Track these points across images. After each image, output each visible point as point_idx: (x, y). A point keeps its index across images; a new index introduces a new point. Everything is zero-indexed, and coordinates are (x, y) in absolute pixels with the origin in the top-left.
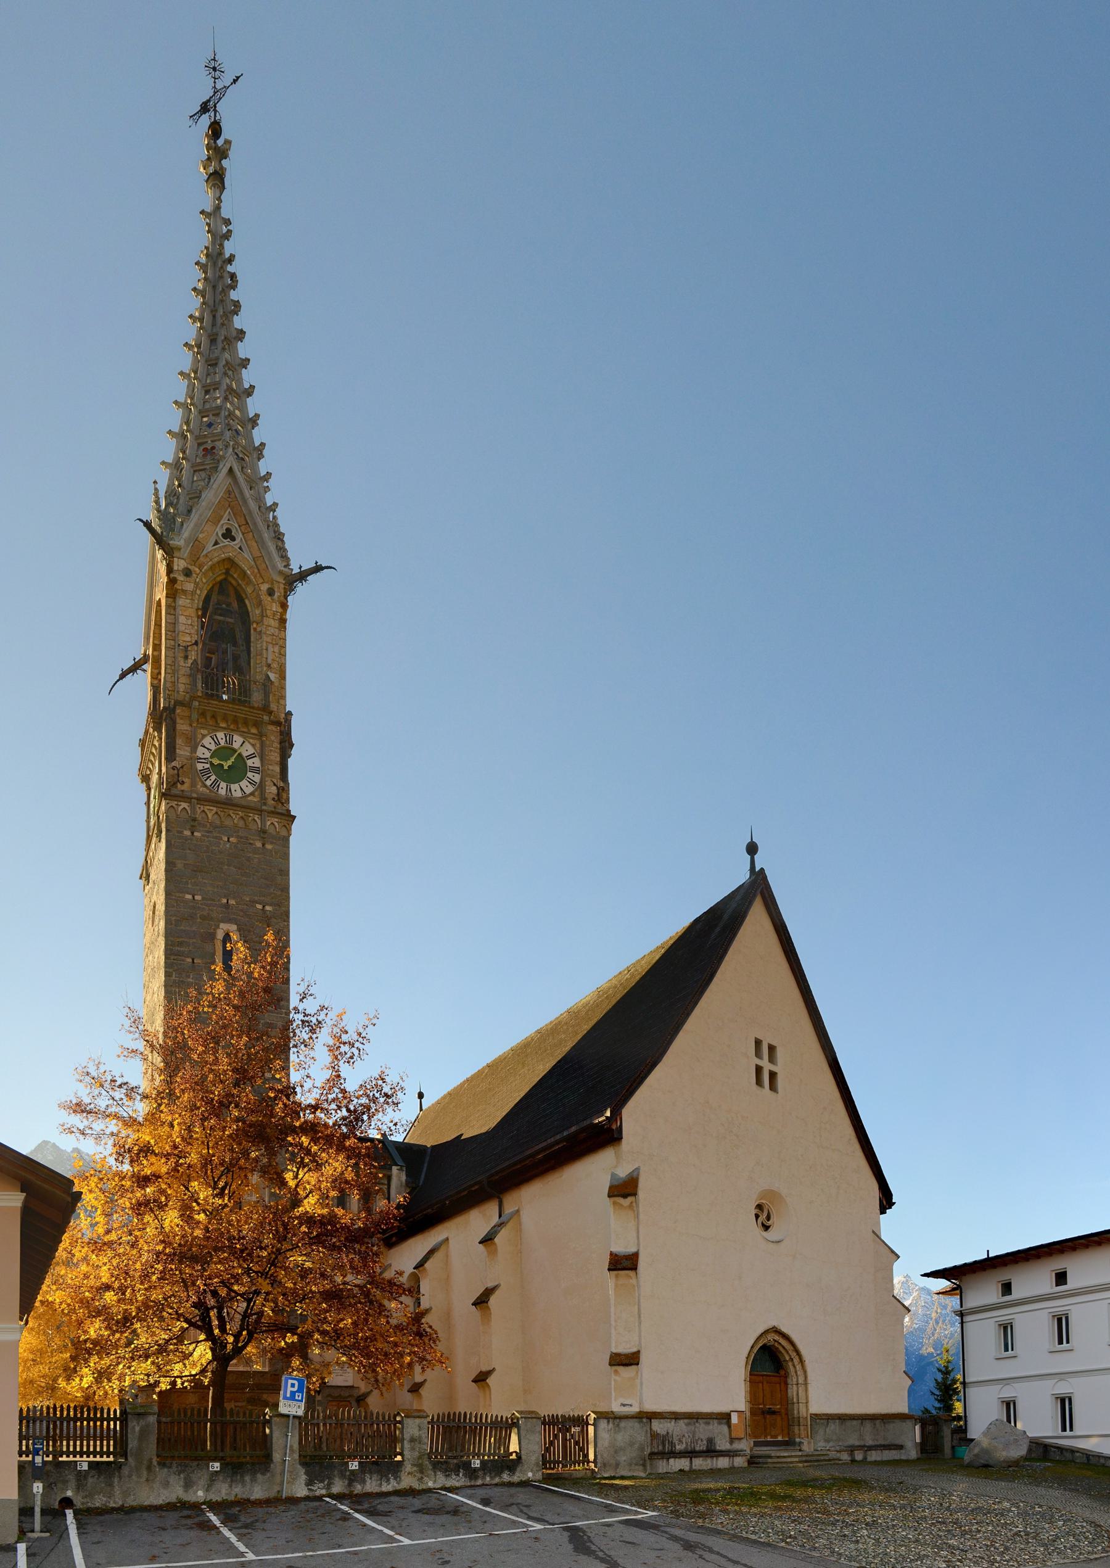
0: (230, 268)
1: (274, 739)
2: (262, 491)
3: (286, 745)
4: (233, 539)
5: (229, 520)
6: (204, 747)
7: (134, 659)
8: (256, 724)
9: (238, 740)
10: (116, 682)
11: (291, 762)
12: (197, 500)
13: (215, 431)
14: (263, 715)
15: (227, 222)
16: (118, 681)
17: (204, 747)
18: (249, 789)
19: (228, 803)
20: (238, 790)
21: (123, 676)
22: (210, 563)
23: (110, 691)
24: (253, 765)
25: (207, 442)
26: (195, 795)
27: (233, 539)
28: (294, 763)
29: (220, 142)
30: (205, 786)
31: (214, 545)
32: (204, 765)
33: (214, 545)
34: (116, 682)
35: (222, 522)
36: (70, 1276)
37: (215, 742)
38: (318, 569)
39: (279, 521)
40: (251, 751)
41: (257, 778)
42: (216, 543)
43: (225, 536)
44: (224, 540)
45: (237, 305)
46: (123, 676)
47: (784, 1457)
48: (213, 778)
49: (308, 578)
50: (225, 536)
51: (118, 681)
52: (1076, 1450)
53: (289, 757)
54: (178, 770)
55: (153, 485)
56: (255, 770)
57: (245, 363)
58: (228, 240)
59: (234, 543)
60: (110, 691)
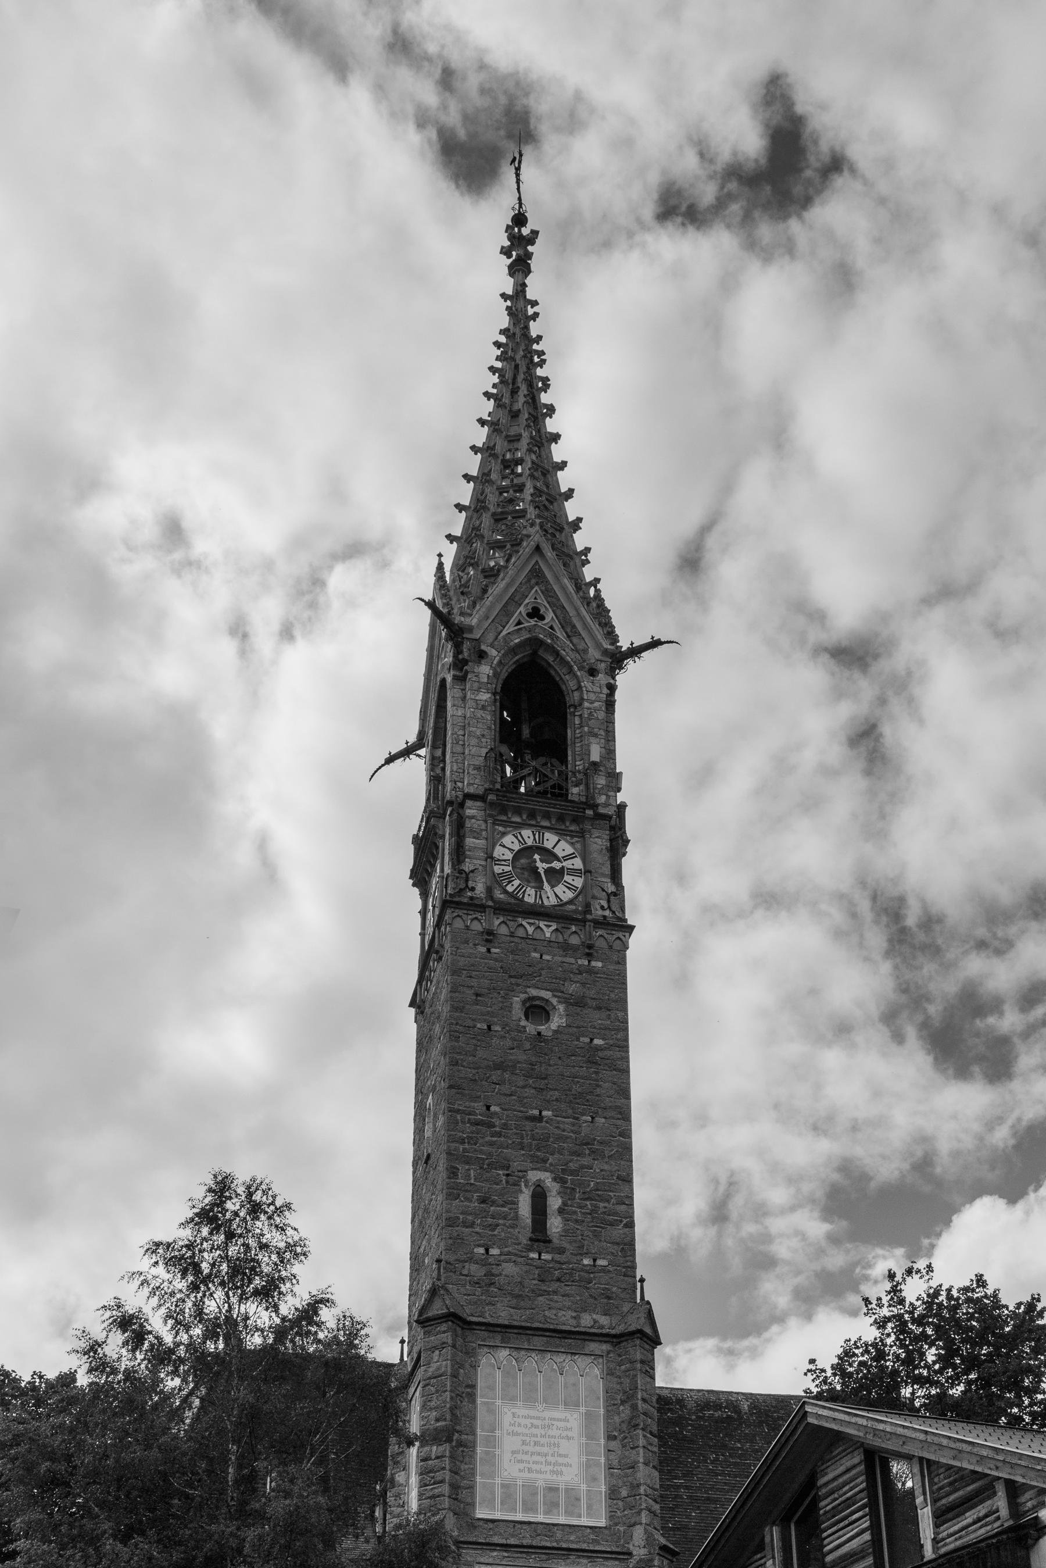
0: (540, 372)
1: (599, 841)
2: (579, 563)
3: (618, 845)
5: (535, 598)
6: (504, 846)
9: (550, 840)
10: (380, 768)
14: (585, 809)
15: (534, 303)
16: (383, 765)
17: (504, 846)
18: (569, 895)
19: (538, 912)
21: (391, 759)
22: (437, 1028)
23: (372, 776)
24: (572, 867)
25: (506, 518)
26: (490, 903)
27: (542, 618)
28: (629, 865)
29: (525, 231)
31: (516, 625)
32: (503, 867)
33: (516, 625)
34: (380, 768)
35: (527, 601)
37: (519, 841)
38: (655, 644)
40: (569, 850)
41: (578, 882)
42: (519, 623)
43: (530, 615)
44: (531, 620)
45: (545, 380)
46: (391, 759)
48: (517, 882)
49: (643, 655)
50: (530, 615)
51: (383, 765)
53: (624, 854)
54: (467, 886)
55: (438, 558)
56: (574, 872)
58: (556, 443)
59: (544, 622)
60: (372, 776)
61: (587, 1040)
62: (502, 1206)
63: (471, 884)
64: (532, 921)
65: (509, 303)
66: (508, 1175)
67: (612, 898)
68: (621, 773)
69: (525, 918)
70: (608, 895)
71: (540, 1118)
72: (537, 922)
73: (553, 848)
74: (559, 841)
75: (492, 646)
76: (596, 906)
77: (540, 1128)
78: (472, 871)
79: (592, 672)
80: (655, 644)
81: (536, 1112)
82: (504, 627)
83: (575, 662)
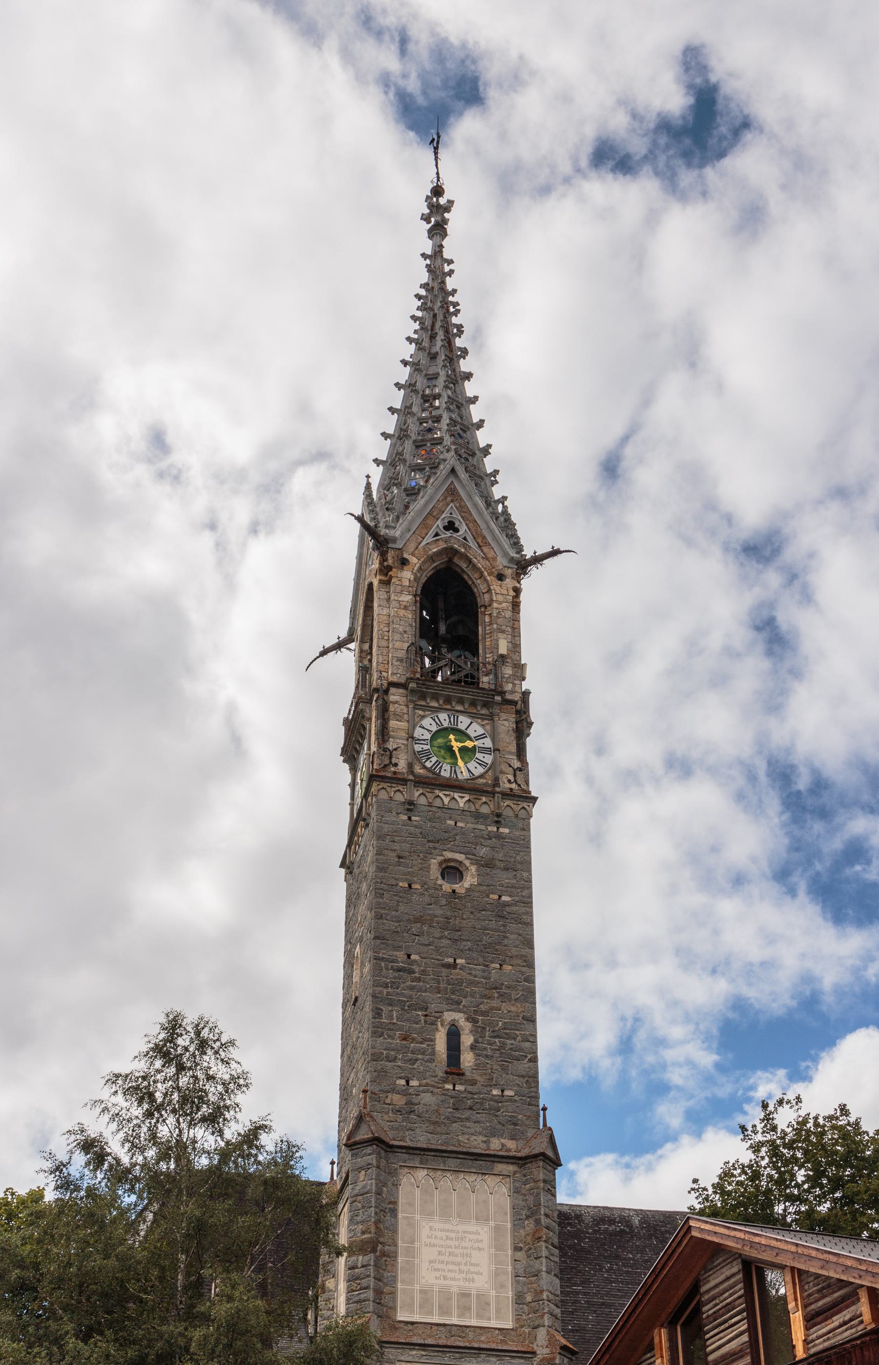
1: (506, 723)
2: (488, 483)
4: (456, 530)
5: (451, 514)
6: (423, 728)
7: (339, 638)
8: (485, 705)
11: (530, 742)
12: (414, 497)
13: (435, 436)
15: (450, 262)
16: (318, 657)
17: (423, 728)
20: (466, 770)
21: (324, 653)
23: (308, 667)
24: (483, 746)
26: (411, 777)
30: (425, 767)
32: (422, 746)
35: (443, 516)
36: (296, 1324)
37: (437, 723)
38: (555, 553)
39: (510, 511)
41: (488, 759)
42: (437, 535)
43: (446, 528)
44: (447, 532)
46: (324, 653)
47: (846, 1330)
49: (544, 562)
50: (446, 528)
51: (318, 657)
52: (757, 1260)
53: (528, 735)
57: (468, 376)
59: (458, 534)
60: (308, 667)
61: (496, 897)
62: (421, 1043)
63: (394, 761)
64: (447, 793)
65: (428, 262)
66: (426, 1016)
67: (518, 772)
68: (525, 664)
69: (442, 790)
70: (515, 770)
71: (454, 966)
72: (452, 793)
73: (466, 729)
74: (472, 723)
75: (413, 554)
76: (503, 779)
77: (456, 974)
78: (396, 749)
79: (501, 577)
80: (555, 553)
81: (451, 960)
82: (424, 538)
83: (485, 568)
